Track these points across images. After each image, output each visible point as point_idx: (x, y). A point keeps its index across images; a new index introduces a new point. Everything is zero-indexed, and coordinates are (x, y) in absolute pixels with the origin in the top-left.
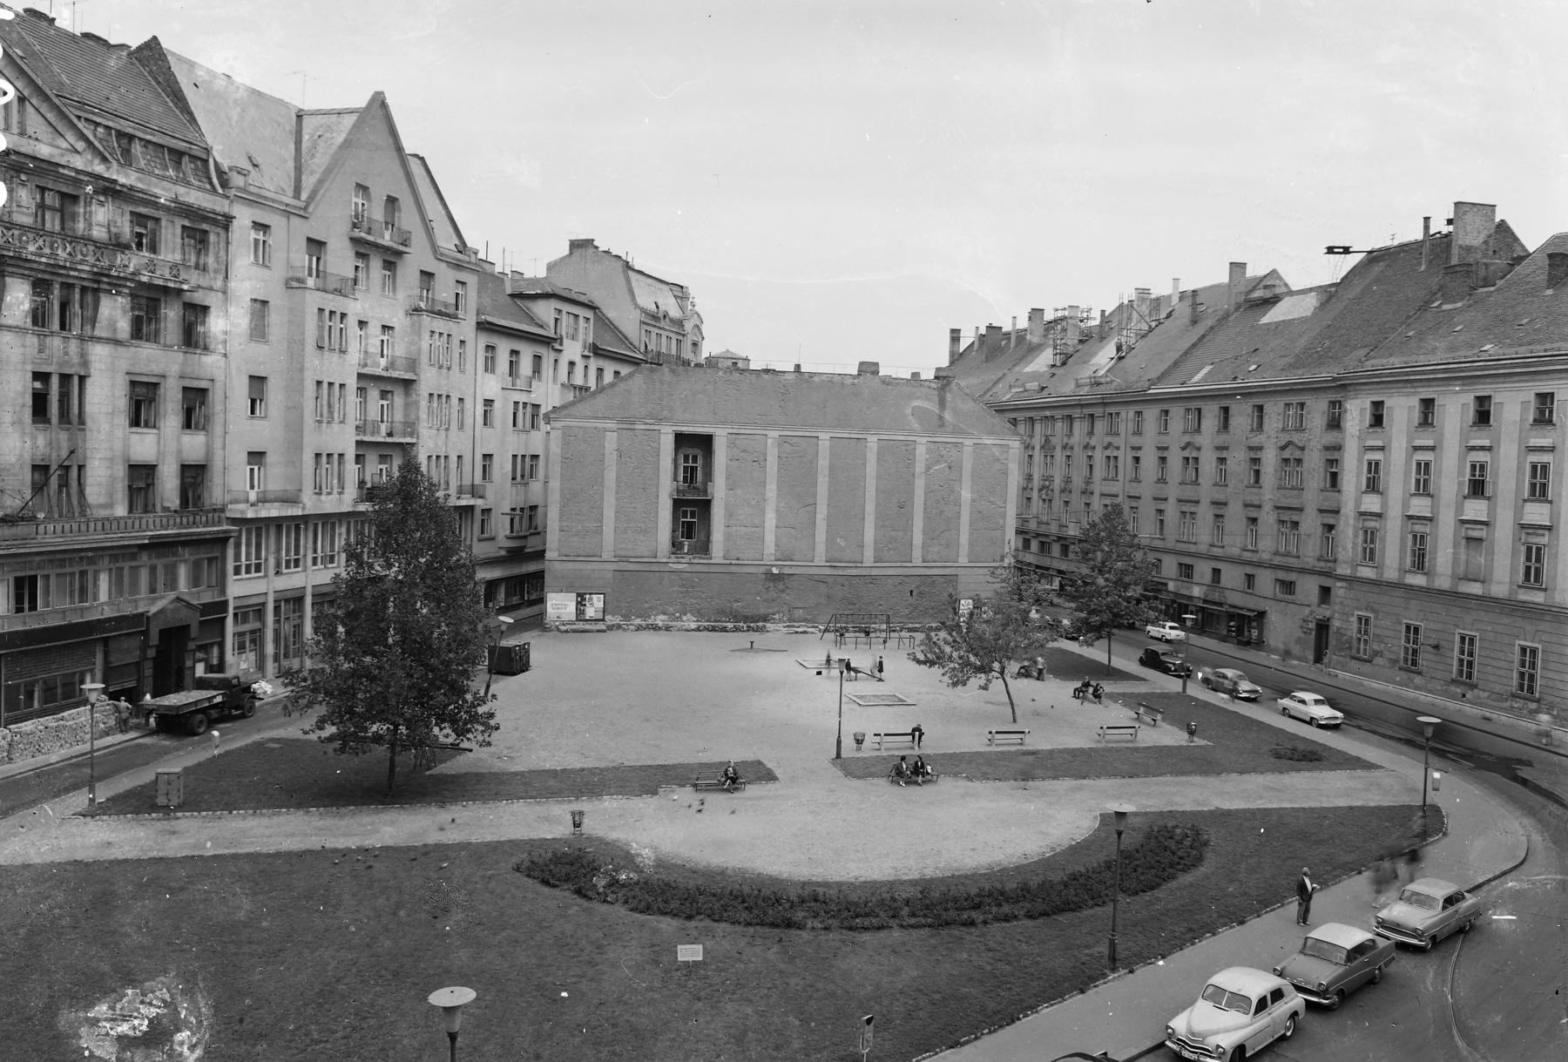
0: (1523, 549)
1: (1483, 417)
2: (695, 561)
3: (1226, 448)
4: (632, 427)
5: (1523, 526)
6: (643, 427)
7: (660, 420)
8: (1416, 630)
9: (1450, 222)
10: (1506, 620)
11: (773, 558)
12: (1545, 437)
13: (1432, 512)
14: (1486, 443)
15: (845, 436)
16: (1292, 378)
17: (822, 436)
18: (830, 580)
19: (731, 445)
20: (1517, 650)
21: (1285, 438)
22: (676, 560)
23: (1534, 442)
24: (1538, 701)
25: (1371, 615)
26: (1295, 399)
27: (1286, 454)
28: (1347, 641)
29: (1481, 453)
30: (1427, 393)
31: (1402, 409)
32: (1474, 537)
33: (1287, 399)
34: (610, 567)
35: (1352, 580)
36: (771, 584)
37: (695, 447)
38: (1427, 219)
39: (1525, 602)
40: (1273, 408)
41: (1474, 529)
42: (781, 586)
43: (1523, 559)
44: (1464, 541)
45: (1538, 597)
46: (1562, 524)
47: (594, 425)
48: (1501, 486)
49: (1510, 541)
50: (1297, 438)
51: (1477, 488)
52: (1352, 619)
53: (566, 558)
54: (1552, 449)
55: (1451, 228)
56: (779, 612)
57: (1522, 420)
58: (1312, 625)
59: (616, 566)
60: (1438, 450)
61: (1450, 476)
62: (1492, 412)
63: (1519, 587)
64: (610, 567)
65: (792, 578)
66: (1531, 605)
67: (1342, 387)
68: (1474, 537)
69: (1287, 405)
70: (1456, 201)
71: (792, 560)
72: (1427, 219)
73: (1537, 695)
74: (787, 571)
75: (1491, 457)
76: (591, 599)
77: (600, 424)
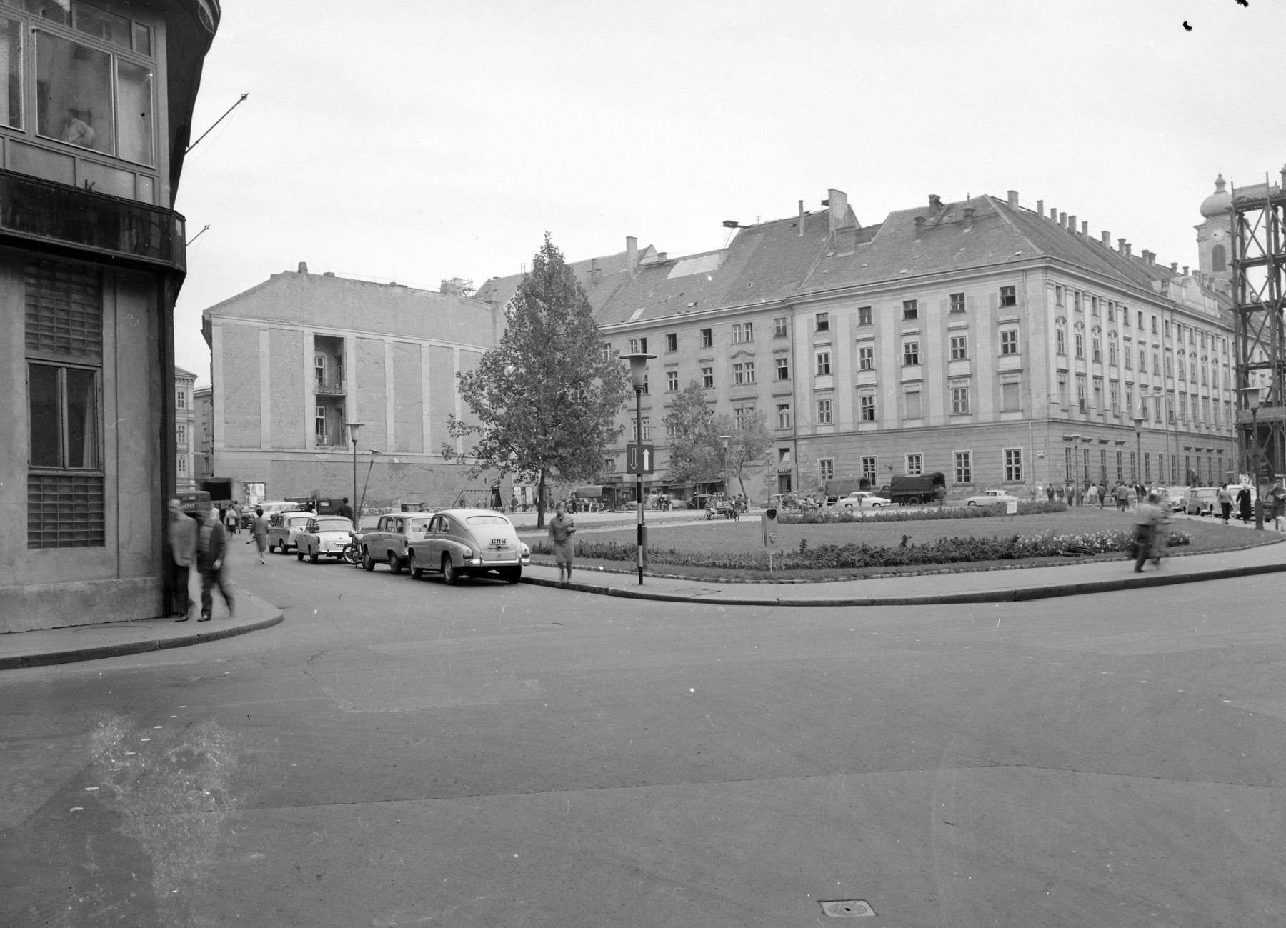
0: (952, 392)
1: (911, 314)
2: (337, 452)
3: (676, 365)
4: (281, 327)
5: (950, 378)
6: (289, 328)
8: (873, 461)
9: (825, 203)
10: (942, 440)
11: (394, 449)
12: (960, 321)
13: (876, 380)
14: (916, 330)
15: (438, 344)
16: (734, 306)
17: (425, 344)
18: (435, 468)
19: (359, 347)
20: (954, 457)
21: (735, 349)
22: (321, 451)
23: (952, 325)
24: (973, 485)
25: (833, 459)
26: (742, 321)
27: (737, 361)
28: (813, 481)
29: (912, 337)
30: (863, 303)
31: (843, 317)
32: (912, 390)
33: (736, 321)
34: (268, 457)
35: (811, 438)
36: (394, 473)
37: (330, 346)
38: (801, 202)
39: (957, 425)
40: (722, 333)
41: (912, 386)
42: (401, 474)
43: (952, 398)
44: (904, 396)
45: (966, 420)
46: (979, 373)
47: (249, 323)
48: (930, 356)
49: (942, 390)
50: (749, 348)
51: (912, 359)
52: (815, 465)
53: (231, 449)
54: (966, 328)
55: (825, 208)
56: (400, 497)
57: (942, 313)
58: (776, 478)
59: (274, 456)
60: (877, 339)
61: (889, 354)
62: (918, 311)
63: (951, 416)
64: (268, 457)
65: (407, 467)
66: (962, 426)
67: (790, 306)
68: (912, 390)
69: (734, 326)
70: (830, 188)
71: (407, 451)
72: (801, 202)
73: (972, 481)
74: (405, 460)
75: (921, 340)
76: (254, 488)
77: (255, 323)
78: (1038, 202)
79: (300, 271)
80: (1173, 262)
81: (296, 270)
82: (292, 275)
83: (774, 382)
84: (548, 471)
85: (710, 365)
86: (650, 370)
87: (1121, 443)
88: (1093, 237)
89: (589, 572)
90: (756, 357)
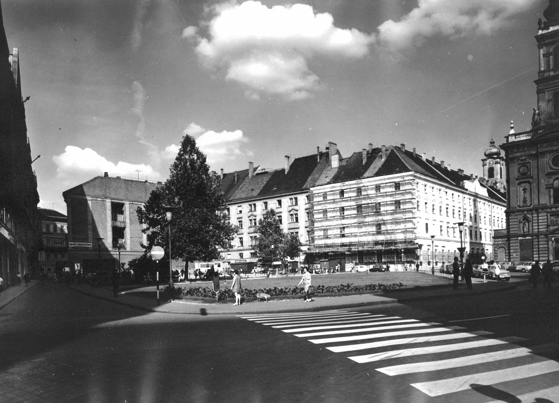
6: (100, 199)
7: (106, 198)
21: (291, 208)
50: (296, 208)
55: (327, 151)
72: (318, 147)
78: (413, 149)
79: (105, 176)
80: (471, 174)
81: (103, 175)
82: (101, 178)
83: (306, 222)
84: (57, 255)
85: (241, 220)
86: (257, 217)
87: (444, 247)
88: (437, 162)
89: (261, 303)
90: (299, 211)
